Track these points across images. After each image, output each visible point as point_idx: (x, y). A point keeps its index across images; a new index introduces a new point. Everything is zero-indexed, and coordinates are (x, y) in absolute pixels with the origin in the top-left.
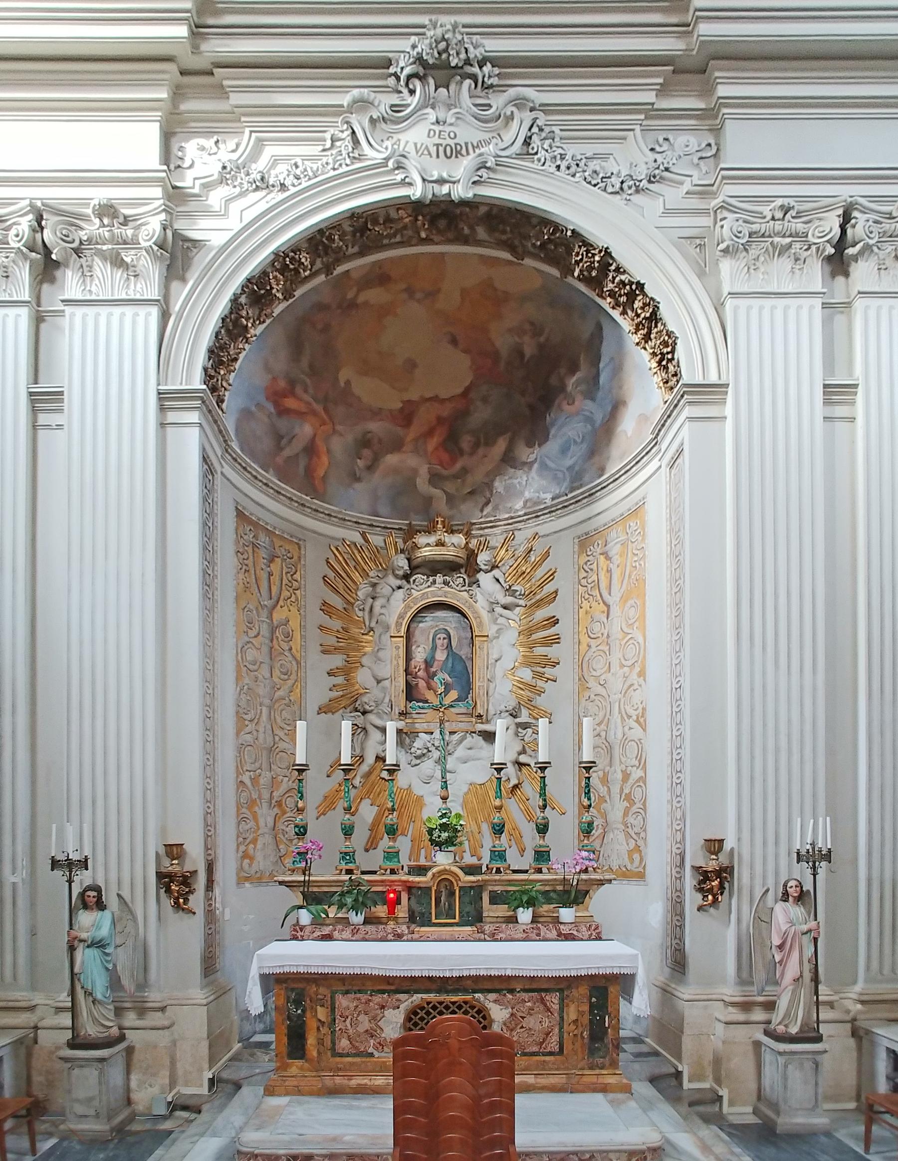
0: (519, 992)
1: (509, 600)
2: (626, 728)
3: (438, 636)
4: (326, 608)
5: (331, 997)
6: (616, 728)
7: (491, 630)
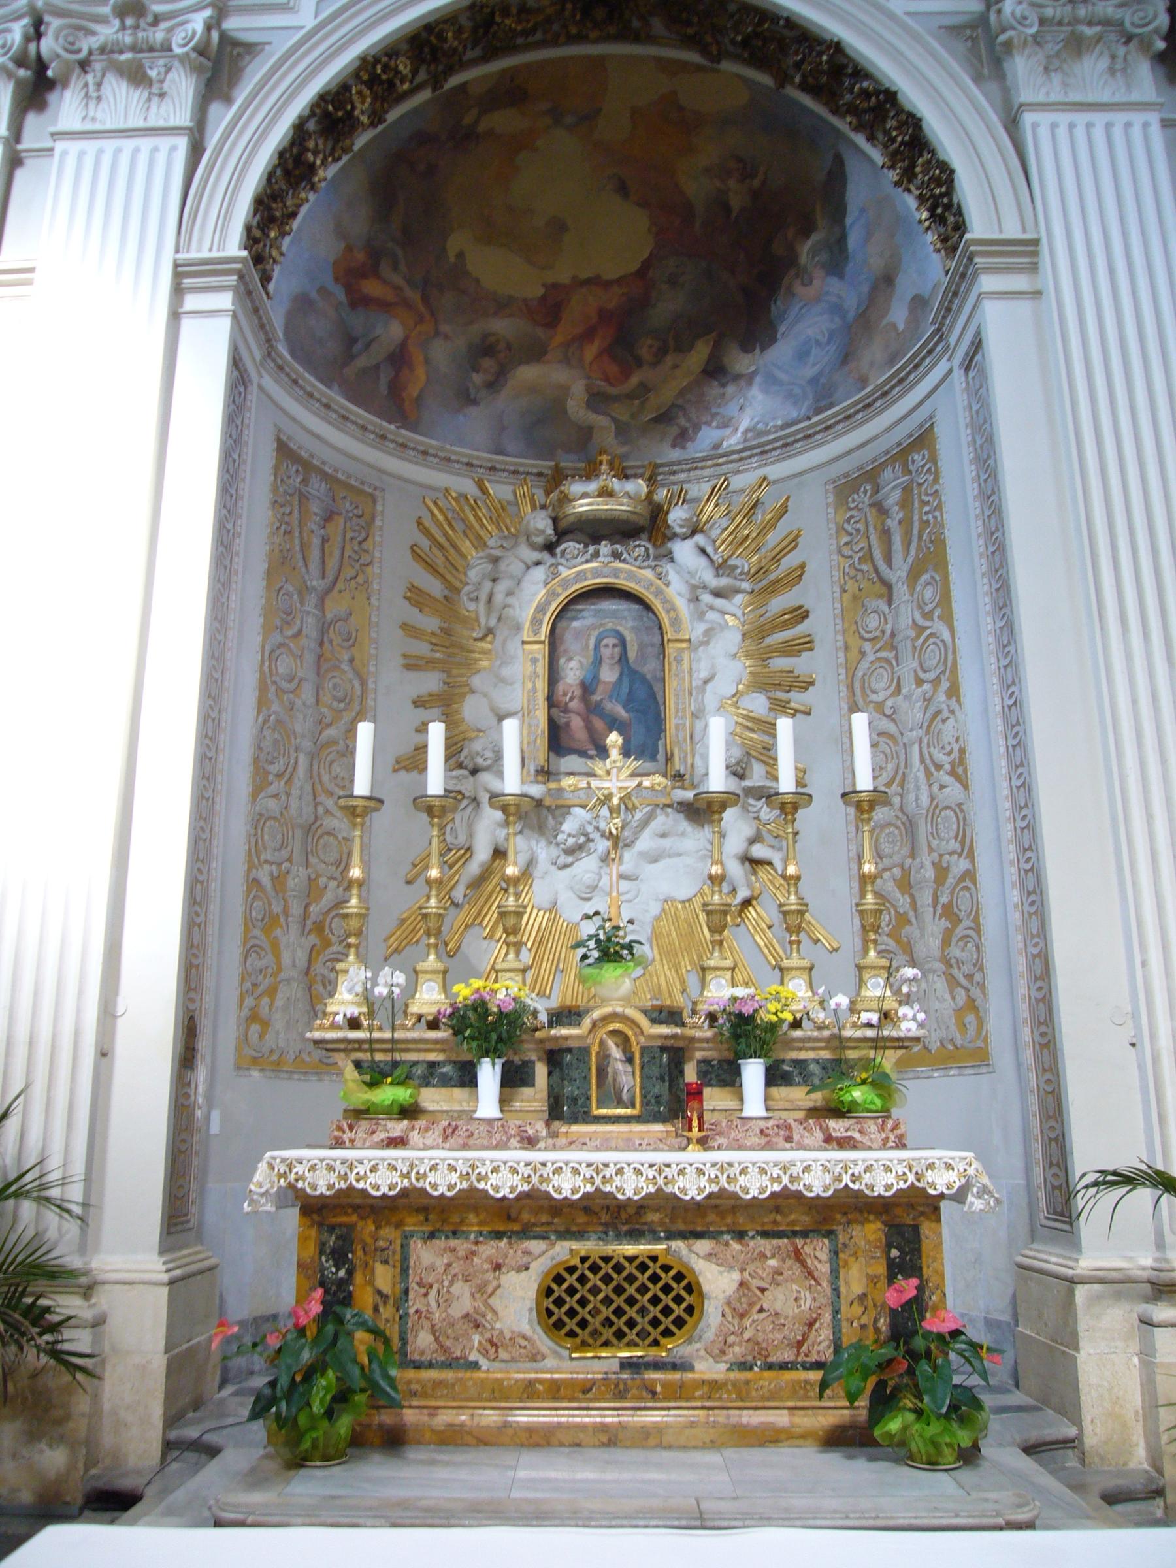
0: (753, 1238)
1: (724, 581)
2: (935, 788)
3: (605, 641)
4: (416, 597)
5: (402, 1246)
6: (918, 788)
7: (697, 631)
